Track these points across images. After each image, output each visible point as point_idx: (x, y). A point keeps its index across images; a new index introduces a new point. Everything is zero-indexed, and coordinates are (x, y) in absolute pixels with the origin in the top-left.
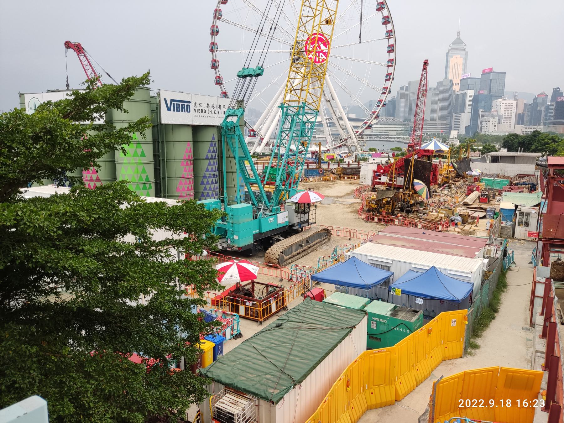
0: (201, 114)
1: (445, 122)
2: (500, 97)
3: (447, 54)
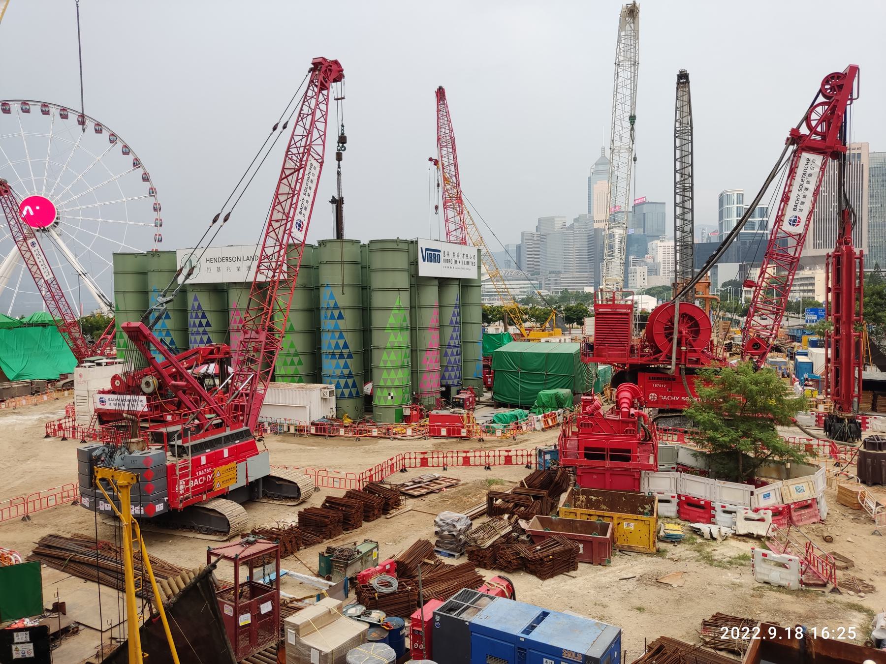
0: (449, 265)
1: (586, 275)
2: (656, 237)
3: (589, 178)
